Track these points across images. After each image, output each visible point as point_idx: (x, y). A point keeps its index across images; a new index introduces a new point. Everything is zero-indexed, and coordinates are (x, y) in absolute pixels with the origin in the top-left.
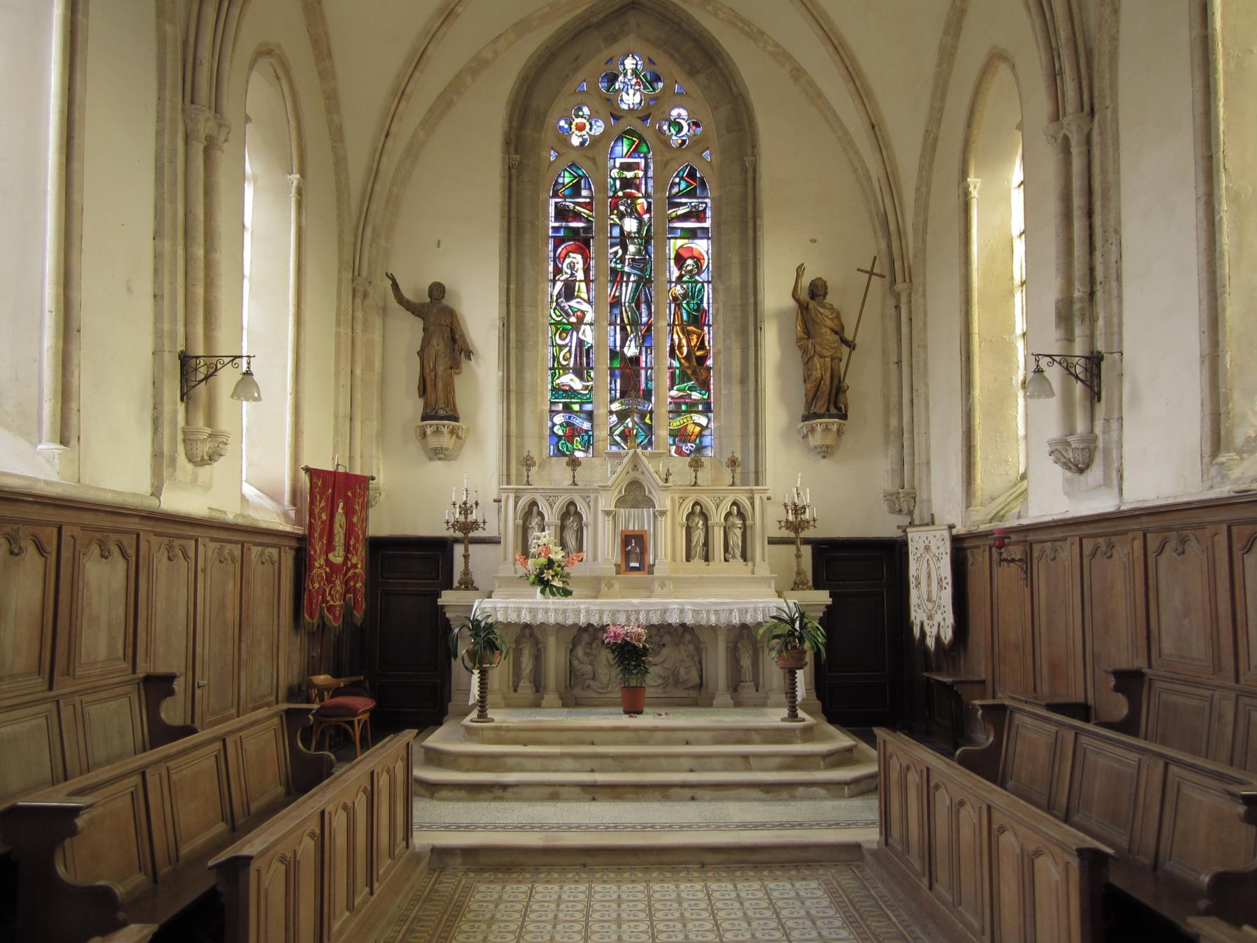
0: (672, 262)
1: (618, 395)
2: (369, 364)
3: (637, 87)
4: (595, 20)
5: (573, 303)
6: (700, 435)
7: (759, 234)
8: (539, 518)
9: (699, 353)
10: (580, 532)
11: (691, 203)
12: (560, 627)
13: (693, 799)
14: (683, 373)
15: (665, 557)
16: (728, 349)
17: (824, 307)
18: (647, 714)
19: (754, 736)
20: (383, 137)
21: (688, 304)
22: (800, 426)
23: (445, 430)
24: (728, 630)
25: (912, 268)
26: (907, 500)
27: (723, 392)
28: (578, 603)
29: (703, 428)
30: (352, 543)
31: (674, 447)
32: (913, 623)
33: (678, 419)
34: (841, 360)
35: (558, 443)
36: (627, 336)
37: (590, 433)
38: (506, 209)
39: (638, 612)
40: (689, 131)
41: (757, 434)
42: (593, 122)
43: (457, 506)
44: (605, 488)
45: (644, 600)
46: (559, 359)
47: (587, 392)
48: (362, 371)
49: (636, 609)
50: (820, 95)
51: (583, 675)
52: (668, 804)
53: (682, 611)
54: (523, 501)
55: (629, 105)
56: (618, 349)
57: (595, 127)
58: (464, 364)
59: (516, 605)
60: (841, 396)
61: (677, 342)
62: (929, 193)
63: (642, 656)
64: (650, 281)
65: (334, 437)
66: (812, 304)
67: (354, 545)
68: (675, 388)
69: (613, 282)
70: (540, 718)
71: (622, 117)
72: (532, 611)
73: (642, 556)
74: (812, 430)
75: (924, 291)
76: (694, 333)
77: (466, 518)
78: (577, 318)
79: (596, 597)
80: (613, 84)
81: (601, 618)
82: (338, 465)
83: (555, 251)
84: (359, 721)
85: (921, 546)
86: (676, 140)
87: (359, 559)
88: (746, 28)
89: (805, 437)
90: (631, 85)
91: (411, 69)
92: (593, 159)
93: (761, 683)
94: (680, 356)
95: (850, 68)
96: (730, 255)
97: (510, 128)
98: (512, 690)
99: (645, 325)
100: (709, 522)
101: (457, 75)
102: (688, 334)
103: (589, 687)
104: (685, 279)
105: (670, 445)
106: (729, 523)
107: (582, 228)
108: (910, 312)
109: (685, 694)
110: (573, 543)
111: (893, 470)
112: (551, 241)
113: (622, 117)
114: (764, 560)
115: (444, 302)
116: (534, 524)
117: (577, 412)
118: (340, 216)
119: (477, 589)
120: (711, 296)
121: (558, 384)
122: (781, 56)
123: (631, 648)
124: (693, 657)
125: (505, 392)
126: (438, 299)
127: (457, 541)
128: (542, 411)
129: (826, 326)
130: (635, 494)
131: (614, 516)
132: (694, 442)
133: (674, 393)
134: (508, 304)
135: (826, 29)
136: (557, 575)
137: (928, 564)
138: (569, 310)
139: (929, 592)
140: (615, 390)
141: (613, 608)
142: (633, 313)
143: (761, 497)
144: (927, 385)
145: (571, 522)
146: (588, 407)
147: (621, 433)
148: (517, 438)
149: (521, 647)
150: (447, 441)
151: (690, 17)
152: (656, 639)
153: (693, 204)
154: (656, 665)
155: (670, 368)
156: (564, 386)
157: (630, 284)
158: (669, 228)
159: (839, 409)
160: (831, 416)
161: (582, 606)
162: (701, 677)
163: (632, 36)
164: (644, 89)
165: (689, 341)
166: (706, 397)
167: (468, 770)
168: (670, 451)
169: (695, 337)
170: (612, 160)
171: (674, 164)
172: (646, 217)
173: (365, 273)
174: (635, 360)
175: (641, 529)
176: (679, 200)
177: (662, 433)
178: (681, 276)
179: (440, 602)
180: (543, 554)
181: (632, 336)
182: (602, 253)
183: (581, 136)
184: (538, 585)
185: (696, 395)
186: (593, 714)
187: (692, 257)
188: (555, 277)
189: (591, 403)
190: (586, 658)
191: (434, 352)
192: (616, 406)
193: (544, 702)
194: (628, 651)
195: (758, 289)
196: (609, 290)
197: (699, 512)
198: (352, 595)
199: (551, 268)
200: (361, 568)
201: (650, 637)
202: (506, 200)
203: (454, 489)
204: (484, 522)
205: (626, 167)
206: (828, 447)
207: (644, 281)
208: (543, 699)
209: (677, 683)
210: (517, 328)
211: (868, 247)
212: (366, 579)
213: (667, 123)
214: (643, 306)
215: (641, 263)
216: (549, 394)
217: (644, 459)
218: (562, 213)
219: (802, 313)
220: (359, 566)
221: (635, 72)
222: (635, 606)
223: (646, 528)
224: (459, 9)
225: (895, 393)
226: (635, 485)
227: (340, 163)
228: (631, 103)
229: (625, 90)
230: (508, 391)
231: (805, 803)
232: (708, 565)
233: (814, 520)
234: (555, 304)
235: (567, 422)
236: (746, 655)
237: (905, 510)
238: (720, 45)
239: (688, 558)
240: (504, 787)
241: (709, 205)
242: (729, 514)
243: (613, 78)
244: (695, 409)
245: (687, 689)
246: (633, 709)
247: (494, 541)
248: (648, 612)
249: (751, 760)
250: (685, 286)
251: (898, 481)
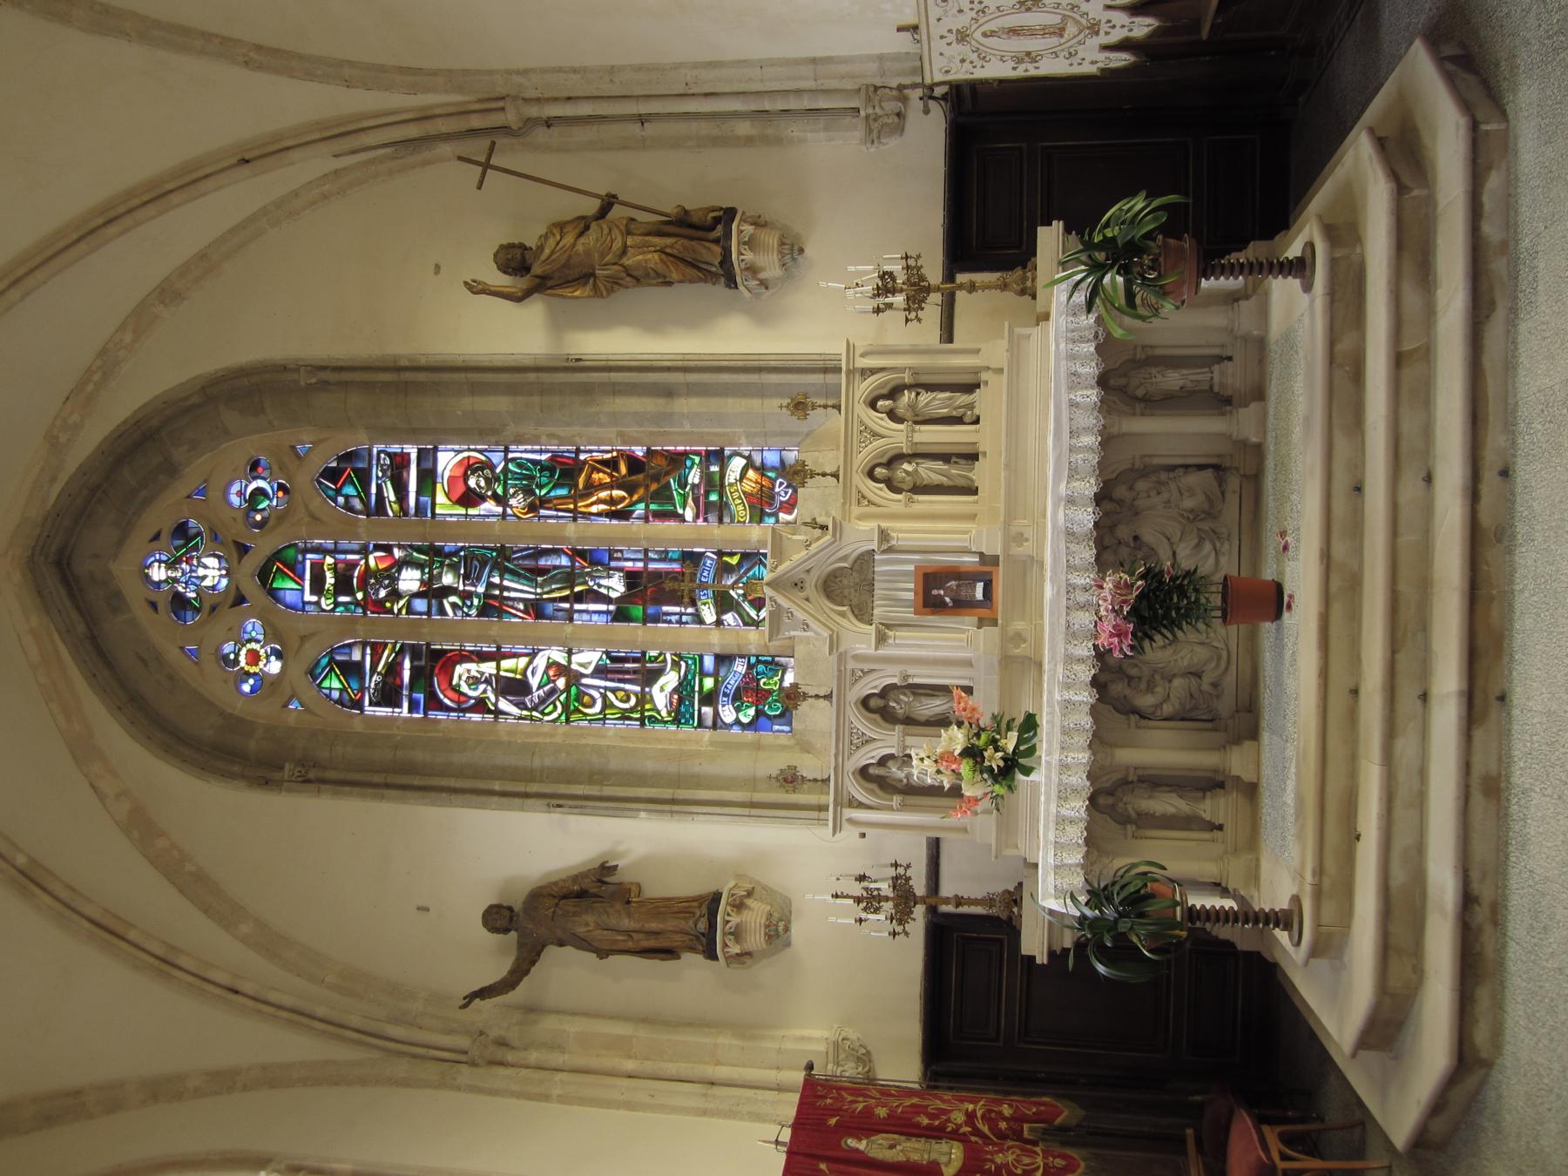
0: (471, 511)
1: (690, 610)
2: (620, 1046)
3: (195, 562)
4: (81, 628)
5: (534, 682)
6: (762, 469)
7: (423, 362)
8: (890, 763)
9: (623, 469)
10: (917, 690)
11: (377, 477)
12: (1099, 741)
13: (1505, 473)
15: (966, 533)
16: (615, 418)
17: (541, 248)
18: (1281, 573)
19: (1345, 345)
20: (235, 997)
21: (541, 487)
22: (746, 294)
23: (735, 919)
24: (1109, 412)
25: (481, 96)
26: (880, 101)
27: (687, 428)
28: (1050, 705)
29: (750, 464)
30: (925, 1121)
31: (783, 516)
32: (1103, 70)
33: (733, 507)
34: (633, 220)
35: (769, 717)
36: (590, 591)
37: (753, 660)
38: (370, 791)
39: (1071, 588)
40: (264, 479)
41: (759, 370)
42: (247, 636)
43: (864, 915)
45: (1048, 574)
46: (626, 710)
47: (683, 664)
48: (630, 1057)
49: (1063, 590)
50: (202, 256)
51: (1191, 695)
52: (1521, 529)
53: (1071, 501)
54: (858, 791)
55: (221, 576)
56: (612, 608)
57: (254, 634)
59: (1052, 826)
60: (695, 219)
61: (602, 507)
62: (351, 64)
63: (1161, 582)
64: (501, 550)
65: (741, 1119)
66: (537, 269)
67: (932, 1117)
68: (680, 511)
69: (500, 613)
70: (1289, 798)
71: (237, 588)
72: (1063, 795)
74: (752, 270)
75: (518, 72)
76: (589, 477)
77: (887, 899)
78: (558, 675)
79: (1040, 665)
80: (188, 601)
81: (1081, 660)
82: (777, 1142)
83: (449, 709)
84: (1284, 1157)
85: (958, 50)
87: (959, 1109)
88: (96, 377)
89: (764, 284)
90: (191, 571)
91: (124, 945)
92: (303, 639)
93: (1216, 351)
94: (627, 501)
95: (145, 198)
96: (459, 413)
97: (243, 777)
98: (1217, 833)
99: (573, 561)
100: (905, 451)
101: (152, 863)
102: (591, 488)
103: (1215, 685)
104: (500, 491)
105: (777, 521)
106: (909, 415)
107: (412, 662)
108: (556, 99)
109: (1233, 499)
110: (938, 702)
111: (826, 129)
112: (432, 714)
113: (237, 588)
114: (978, 351)
115: (518, 906)
116: (901, 775)
117: (716, 682)
118: (363, 1082)
119: (1020, 884)
120: (529, 447)
121: (669, 713)
122: (140, 320)
123: (1145, 603)
124: (1160, 483)
125: (676, 808)
126: (511, 919)
127: (932, 910)
128: (712, 743)
129: (574, 245)
131: (888, 626)
132: (773, 481)
133: (689, 514)
134: (527, 795)
135: (75, 236)
136: (994, 742)
137: (992, 34)
138: (546, 689)
139: (1046, 31)
140: (681, 614)
141: (1061, 637)
142: (552, 580)
143: (862, 356)
144: (677, 67)
146: (709, 662)
147: (755, 608)
148: (755, 790)
149: (1133, 815)
150: (755, 916)
151: (82, 471)
152: (1124, 552)
153: (380, 474)
154: (1174, 554)
155: (646, 519)
156: (671, 703)
157: (506, 583)
158: (416, 514)
159: (717, 220)
160: (728, 235)
161: (1057, 696)
162: (1200, 467)
163: (113, 567)
164: (197, 550)
165: (603, 487)
166: (697, 459)
167: (1419, 971)
168: (788, 523)
169: (595, 476)
170: (307, 608)
172: (397, 553)
173: (462, 1042)
174: (632, 578)
175: (912, 579)
176: (373, 498)
177: (756, 534)
178: (495, 497)
179: (1042, 958)
180: (954, 767)
181: (591, 583)
182: (453, 631)
183: (268, 657)
184: (1013, 779)
185: (694, 477)
186: (1279, 682)
187: (466, 478)
188: (489, 711)
189: (701, 657)
190: (1159, 689)
191: (599, 932)
192: (709, 615)
193: (1248, 777)
194: (1151, 608)
195: (513, 364)
196: (513, 620)
197: (886, 469)
198: (1026, 1126)
199: (476, 717)
200: (974, 1102)
201: (1122, 565)
202: (356, 790)
203: (832, 919)
204: (896, 865)
205: (318, 586)
206: (782, 244)
207: (502, 560)
208: (1238, 778)
209: (1211, 514)
210: (569, 782)
212: (996, 1092)
213: (252, 514)
214: (543, 562)
215: (471, 565)
216: (685, 728)
217: (781, 568)
218: (389, 696)
219: (551, 288)
220: (971, 1107)
221: (171, 565)
222: (1058, 593)
223: (911, 568)
224: (21, 860)
225: (694, 127)
226: (831, 587)
227: (273, 1078)
228: (219, 573)
229: (198, 582)
230: (674, 802)
231: (1525, 213)
232: (985, 454)
233: (907, 257)
234: (534, 713)
235: (734, 700)
236: (1160, 378)
237: (892, 106)
238: (125, 422)
240: (1468, 900)
241: (382, 447)
242: (892, 415)
243: (179, 602)
244: (717, 477)
245: (1223, 493)
246: (1274, 601)
247: (935, 847)
248: (1071, 568)
249: (1407, 346)
250: (512, 491)
251: (847, 120)
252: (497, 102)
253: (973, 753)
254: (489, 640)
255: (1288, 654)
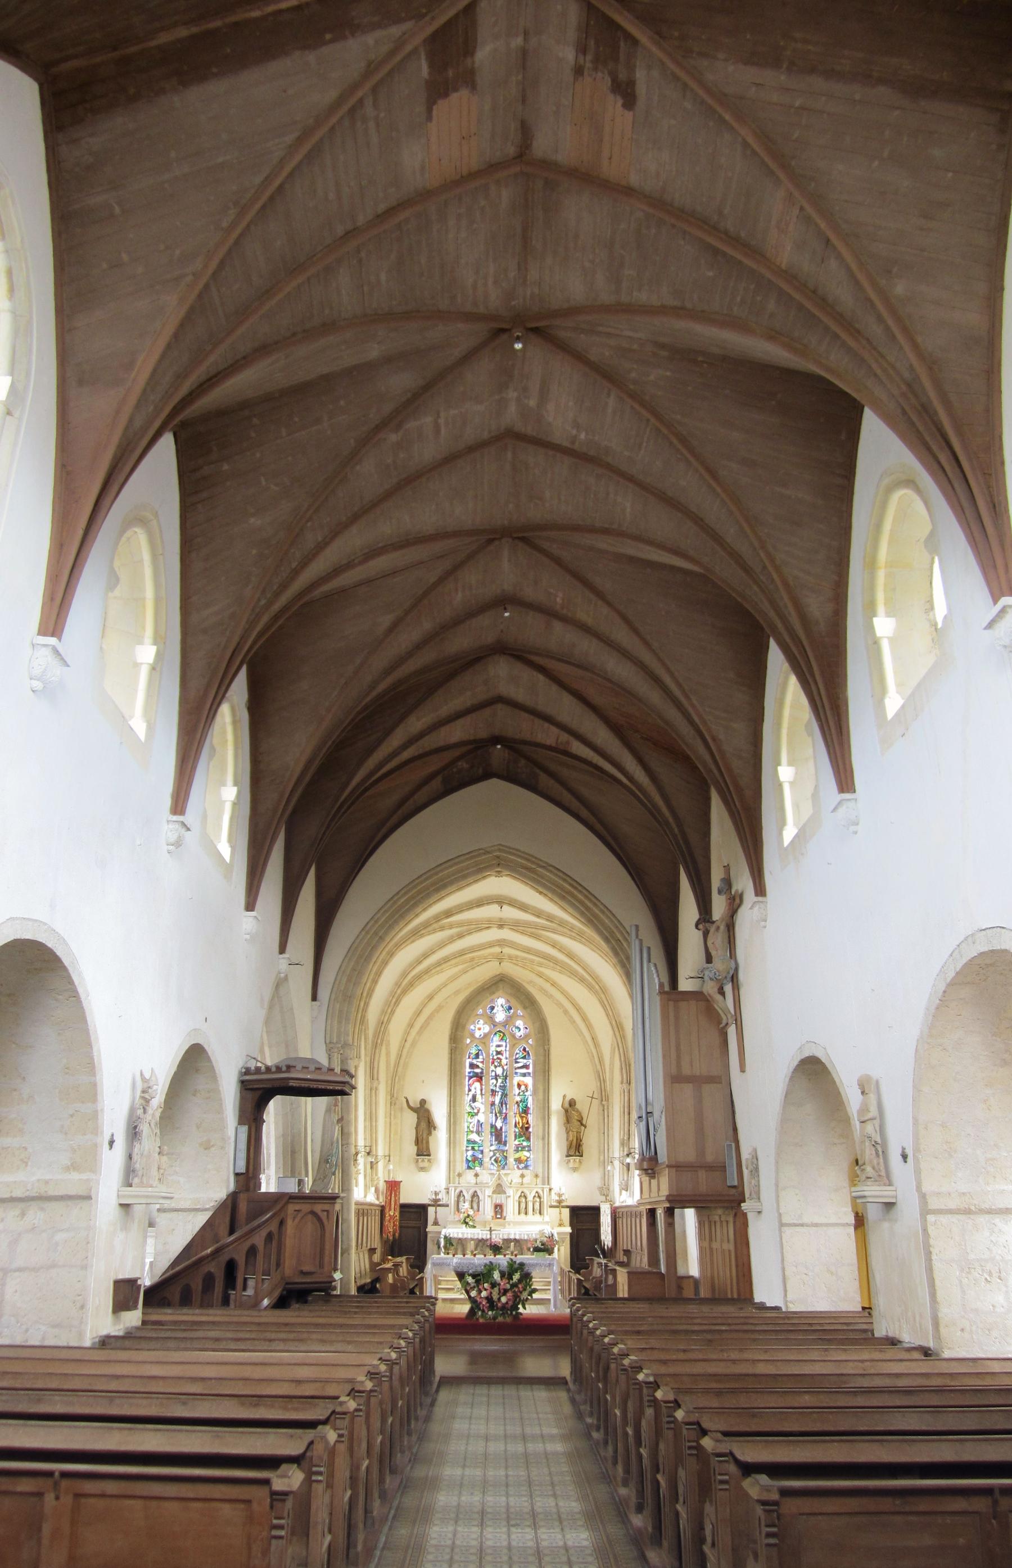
6: (527, 1160)
14: (520, 1134)
44: (488, 1187)
54: (458, 1191)
58: (433, 1132)
64: (506, 1095)
69: (492, 1095)
73: (501, 1213)
86: (518, 1034)
102: (522, 1117)
130: (499, 1189)
145: (475, 1198)
146: (481, 1148)
171: (517, 1046)
177: (511, 1160)
185: (525, 1144)
207: (504, 1095)
211: (593, 1086)
215: (503, 1088)
218: (472, 1066)
226: (499, 1186)
239: (519, 1213)
242: (535, 1196)
243: (493, 1008)
252: (607, 1100)
253: (468, 1216)
254: (486, 1092)
255: (556, 899)
